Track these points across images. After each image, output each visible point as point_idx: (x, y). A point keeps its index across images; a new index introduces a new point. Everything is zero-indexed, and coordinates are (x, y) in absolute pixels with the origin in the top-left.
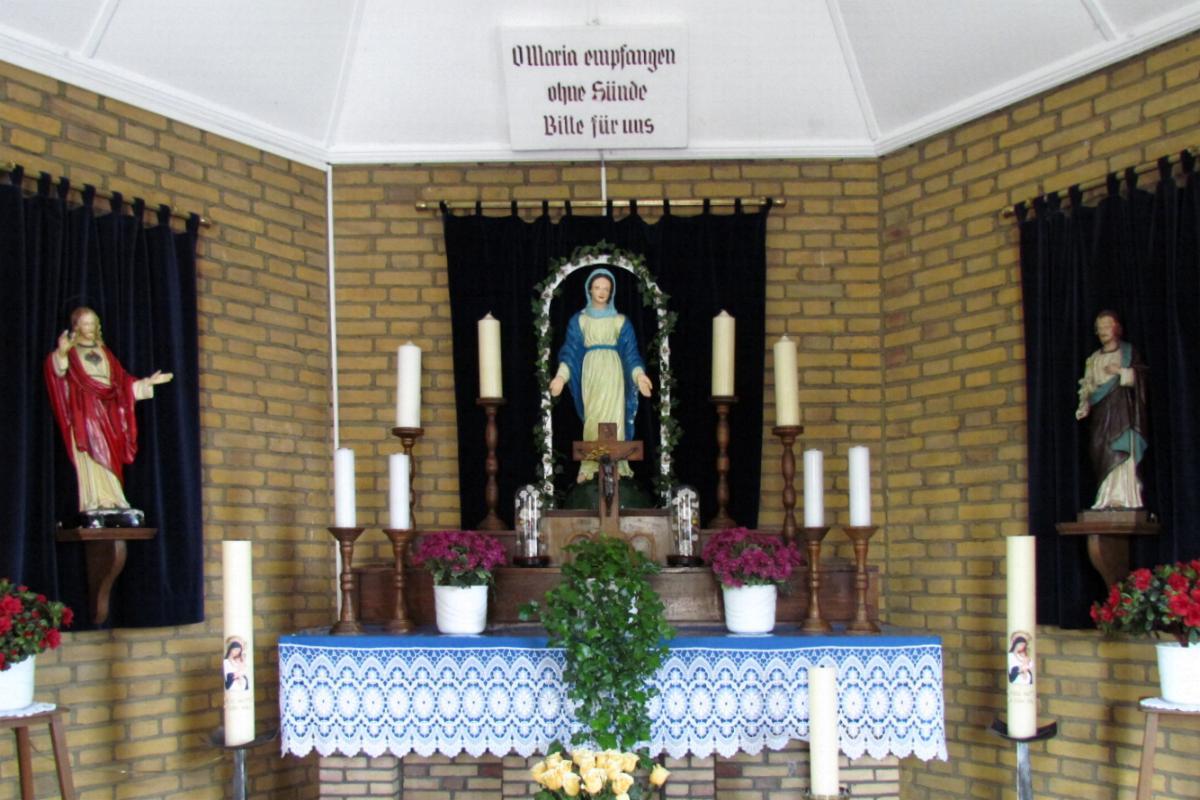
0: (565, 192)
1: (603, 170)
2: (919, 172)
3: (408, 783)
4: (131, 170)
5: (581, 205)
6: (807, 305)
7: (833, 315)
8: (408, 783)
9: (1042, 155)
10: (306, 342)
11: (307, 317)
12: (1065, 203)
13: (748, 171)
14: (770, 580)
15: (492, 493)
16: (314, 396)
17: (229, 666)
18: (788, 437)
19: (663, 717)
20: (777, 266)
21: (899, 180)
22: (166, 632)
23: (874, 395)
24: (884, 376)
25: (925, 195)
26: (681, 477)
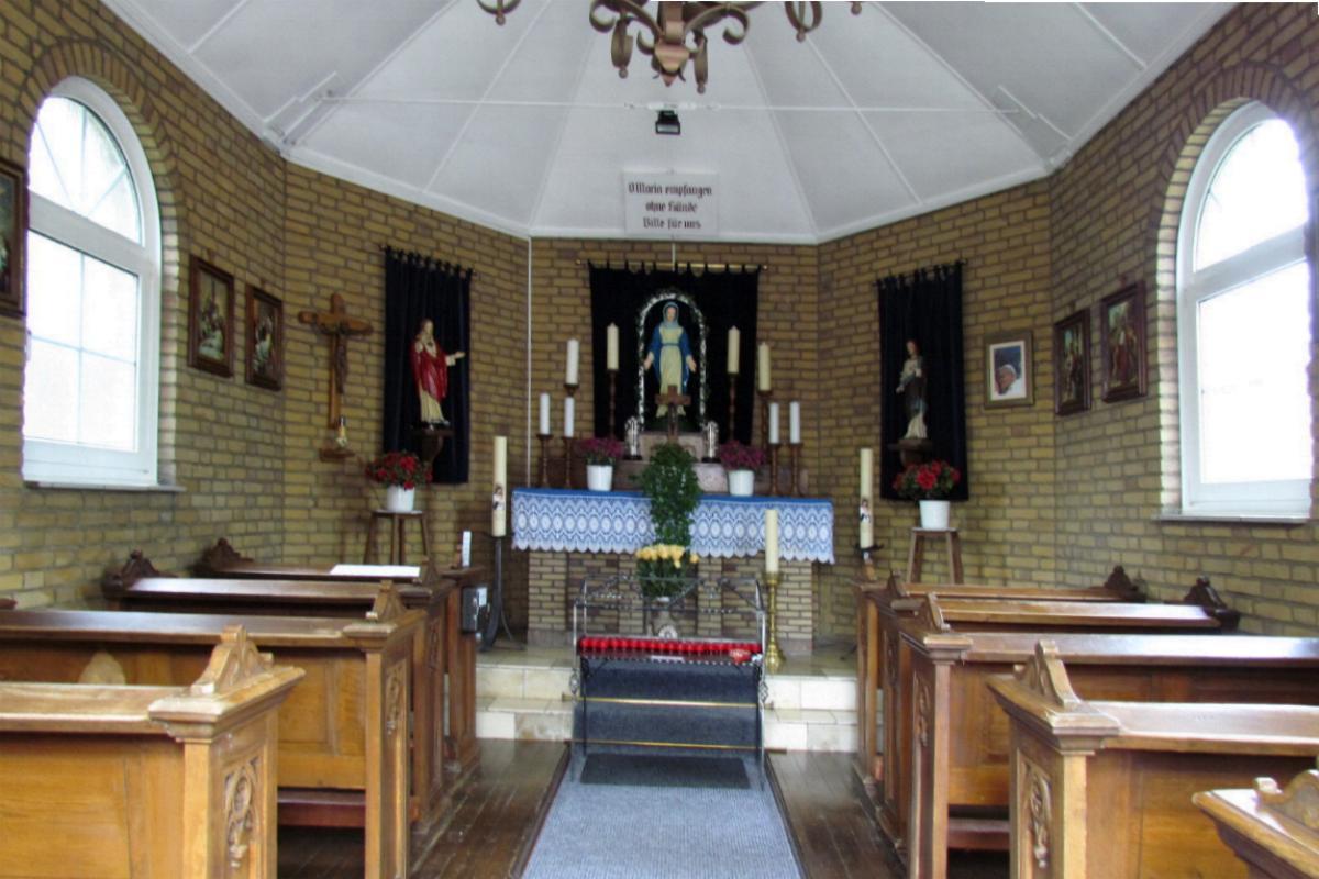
0: (653, 257)
2: (838, 255)
5: (661, 265)
10: (516, 335)
11: (517, 321)
13: (750, 249)
15: (612, 422)
17: (496, 498)
18: (767, 397)
26: (710, 416)
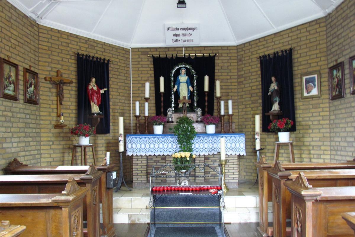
0: (176, 52)
1: (184, 48)
2: (244, 49)
3: (148, 161)
4: (98, 52)
6: (223, 73)
7: (228, 75)
8: (148, 161)
9: (264, 48)
10: (126, 82)
11: (126, 77)
12: (267, 57)
13: (212, 48)
14: (214, 124)
15: (162, 110)
16: (127, 92)
17: (120, 139)
19: (195, 148)
20: (217, 66)
21: (240, 50)
22: (103, 135)
23: (236, 91)
24: (238, 87)
25: (245, 53)
26: (198, 106)
